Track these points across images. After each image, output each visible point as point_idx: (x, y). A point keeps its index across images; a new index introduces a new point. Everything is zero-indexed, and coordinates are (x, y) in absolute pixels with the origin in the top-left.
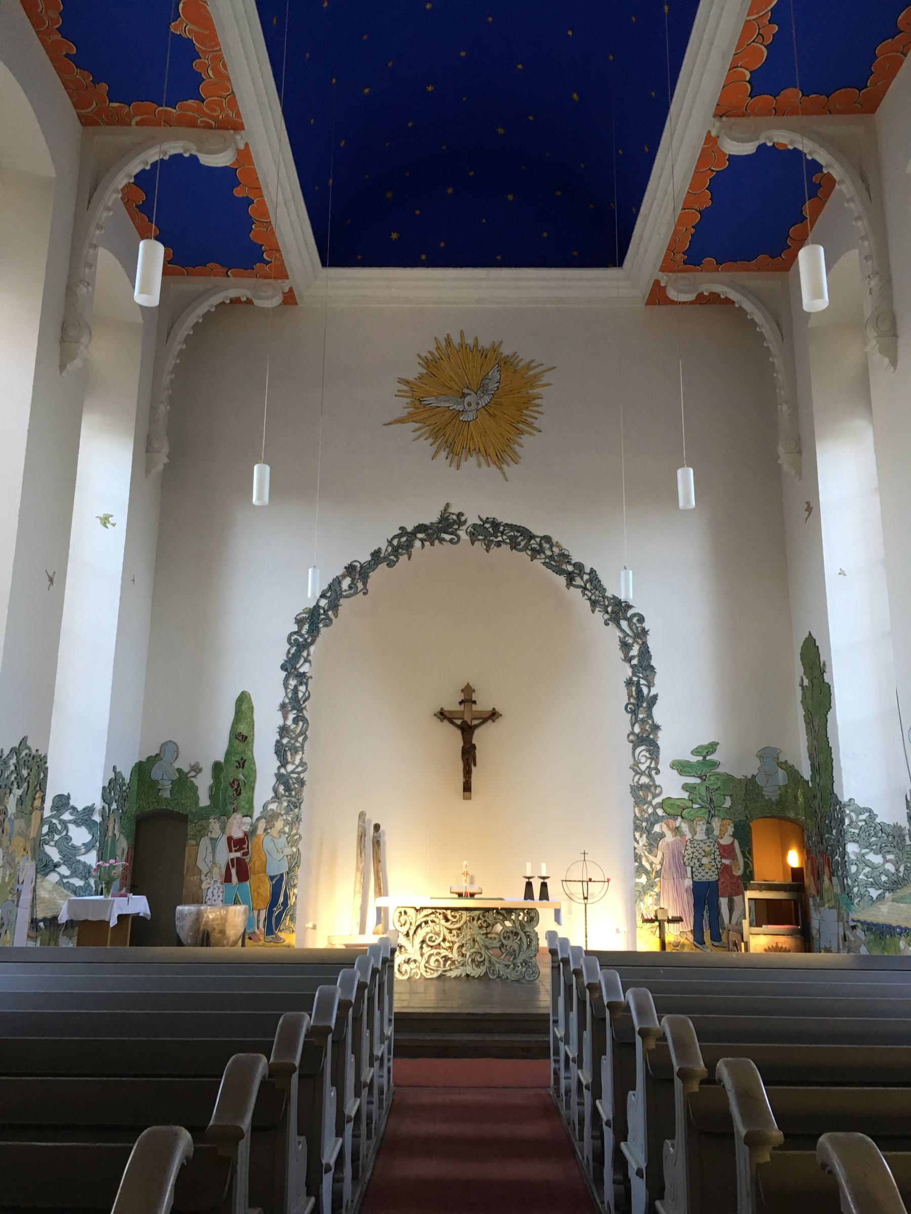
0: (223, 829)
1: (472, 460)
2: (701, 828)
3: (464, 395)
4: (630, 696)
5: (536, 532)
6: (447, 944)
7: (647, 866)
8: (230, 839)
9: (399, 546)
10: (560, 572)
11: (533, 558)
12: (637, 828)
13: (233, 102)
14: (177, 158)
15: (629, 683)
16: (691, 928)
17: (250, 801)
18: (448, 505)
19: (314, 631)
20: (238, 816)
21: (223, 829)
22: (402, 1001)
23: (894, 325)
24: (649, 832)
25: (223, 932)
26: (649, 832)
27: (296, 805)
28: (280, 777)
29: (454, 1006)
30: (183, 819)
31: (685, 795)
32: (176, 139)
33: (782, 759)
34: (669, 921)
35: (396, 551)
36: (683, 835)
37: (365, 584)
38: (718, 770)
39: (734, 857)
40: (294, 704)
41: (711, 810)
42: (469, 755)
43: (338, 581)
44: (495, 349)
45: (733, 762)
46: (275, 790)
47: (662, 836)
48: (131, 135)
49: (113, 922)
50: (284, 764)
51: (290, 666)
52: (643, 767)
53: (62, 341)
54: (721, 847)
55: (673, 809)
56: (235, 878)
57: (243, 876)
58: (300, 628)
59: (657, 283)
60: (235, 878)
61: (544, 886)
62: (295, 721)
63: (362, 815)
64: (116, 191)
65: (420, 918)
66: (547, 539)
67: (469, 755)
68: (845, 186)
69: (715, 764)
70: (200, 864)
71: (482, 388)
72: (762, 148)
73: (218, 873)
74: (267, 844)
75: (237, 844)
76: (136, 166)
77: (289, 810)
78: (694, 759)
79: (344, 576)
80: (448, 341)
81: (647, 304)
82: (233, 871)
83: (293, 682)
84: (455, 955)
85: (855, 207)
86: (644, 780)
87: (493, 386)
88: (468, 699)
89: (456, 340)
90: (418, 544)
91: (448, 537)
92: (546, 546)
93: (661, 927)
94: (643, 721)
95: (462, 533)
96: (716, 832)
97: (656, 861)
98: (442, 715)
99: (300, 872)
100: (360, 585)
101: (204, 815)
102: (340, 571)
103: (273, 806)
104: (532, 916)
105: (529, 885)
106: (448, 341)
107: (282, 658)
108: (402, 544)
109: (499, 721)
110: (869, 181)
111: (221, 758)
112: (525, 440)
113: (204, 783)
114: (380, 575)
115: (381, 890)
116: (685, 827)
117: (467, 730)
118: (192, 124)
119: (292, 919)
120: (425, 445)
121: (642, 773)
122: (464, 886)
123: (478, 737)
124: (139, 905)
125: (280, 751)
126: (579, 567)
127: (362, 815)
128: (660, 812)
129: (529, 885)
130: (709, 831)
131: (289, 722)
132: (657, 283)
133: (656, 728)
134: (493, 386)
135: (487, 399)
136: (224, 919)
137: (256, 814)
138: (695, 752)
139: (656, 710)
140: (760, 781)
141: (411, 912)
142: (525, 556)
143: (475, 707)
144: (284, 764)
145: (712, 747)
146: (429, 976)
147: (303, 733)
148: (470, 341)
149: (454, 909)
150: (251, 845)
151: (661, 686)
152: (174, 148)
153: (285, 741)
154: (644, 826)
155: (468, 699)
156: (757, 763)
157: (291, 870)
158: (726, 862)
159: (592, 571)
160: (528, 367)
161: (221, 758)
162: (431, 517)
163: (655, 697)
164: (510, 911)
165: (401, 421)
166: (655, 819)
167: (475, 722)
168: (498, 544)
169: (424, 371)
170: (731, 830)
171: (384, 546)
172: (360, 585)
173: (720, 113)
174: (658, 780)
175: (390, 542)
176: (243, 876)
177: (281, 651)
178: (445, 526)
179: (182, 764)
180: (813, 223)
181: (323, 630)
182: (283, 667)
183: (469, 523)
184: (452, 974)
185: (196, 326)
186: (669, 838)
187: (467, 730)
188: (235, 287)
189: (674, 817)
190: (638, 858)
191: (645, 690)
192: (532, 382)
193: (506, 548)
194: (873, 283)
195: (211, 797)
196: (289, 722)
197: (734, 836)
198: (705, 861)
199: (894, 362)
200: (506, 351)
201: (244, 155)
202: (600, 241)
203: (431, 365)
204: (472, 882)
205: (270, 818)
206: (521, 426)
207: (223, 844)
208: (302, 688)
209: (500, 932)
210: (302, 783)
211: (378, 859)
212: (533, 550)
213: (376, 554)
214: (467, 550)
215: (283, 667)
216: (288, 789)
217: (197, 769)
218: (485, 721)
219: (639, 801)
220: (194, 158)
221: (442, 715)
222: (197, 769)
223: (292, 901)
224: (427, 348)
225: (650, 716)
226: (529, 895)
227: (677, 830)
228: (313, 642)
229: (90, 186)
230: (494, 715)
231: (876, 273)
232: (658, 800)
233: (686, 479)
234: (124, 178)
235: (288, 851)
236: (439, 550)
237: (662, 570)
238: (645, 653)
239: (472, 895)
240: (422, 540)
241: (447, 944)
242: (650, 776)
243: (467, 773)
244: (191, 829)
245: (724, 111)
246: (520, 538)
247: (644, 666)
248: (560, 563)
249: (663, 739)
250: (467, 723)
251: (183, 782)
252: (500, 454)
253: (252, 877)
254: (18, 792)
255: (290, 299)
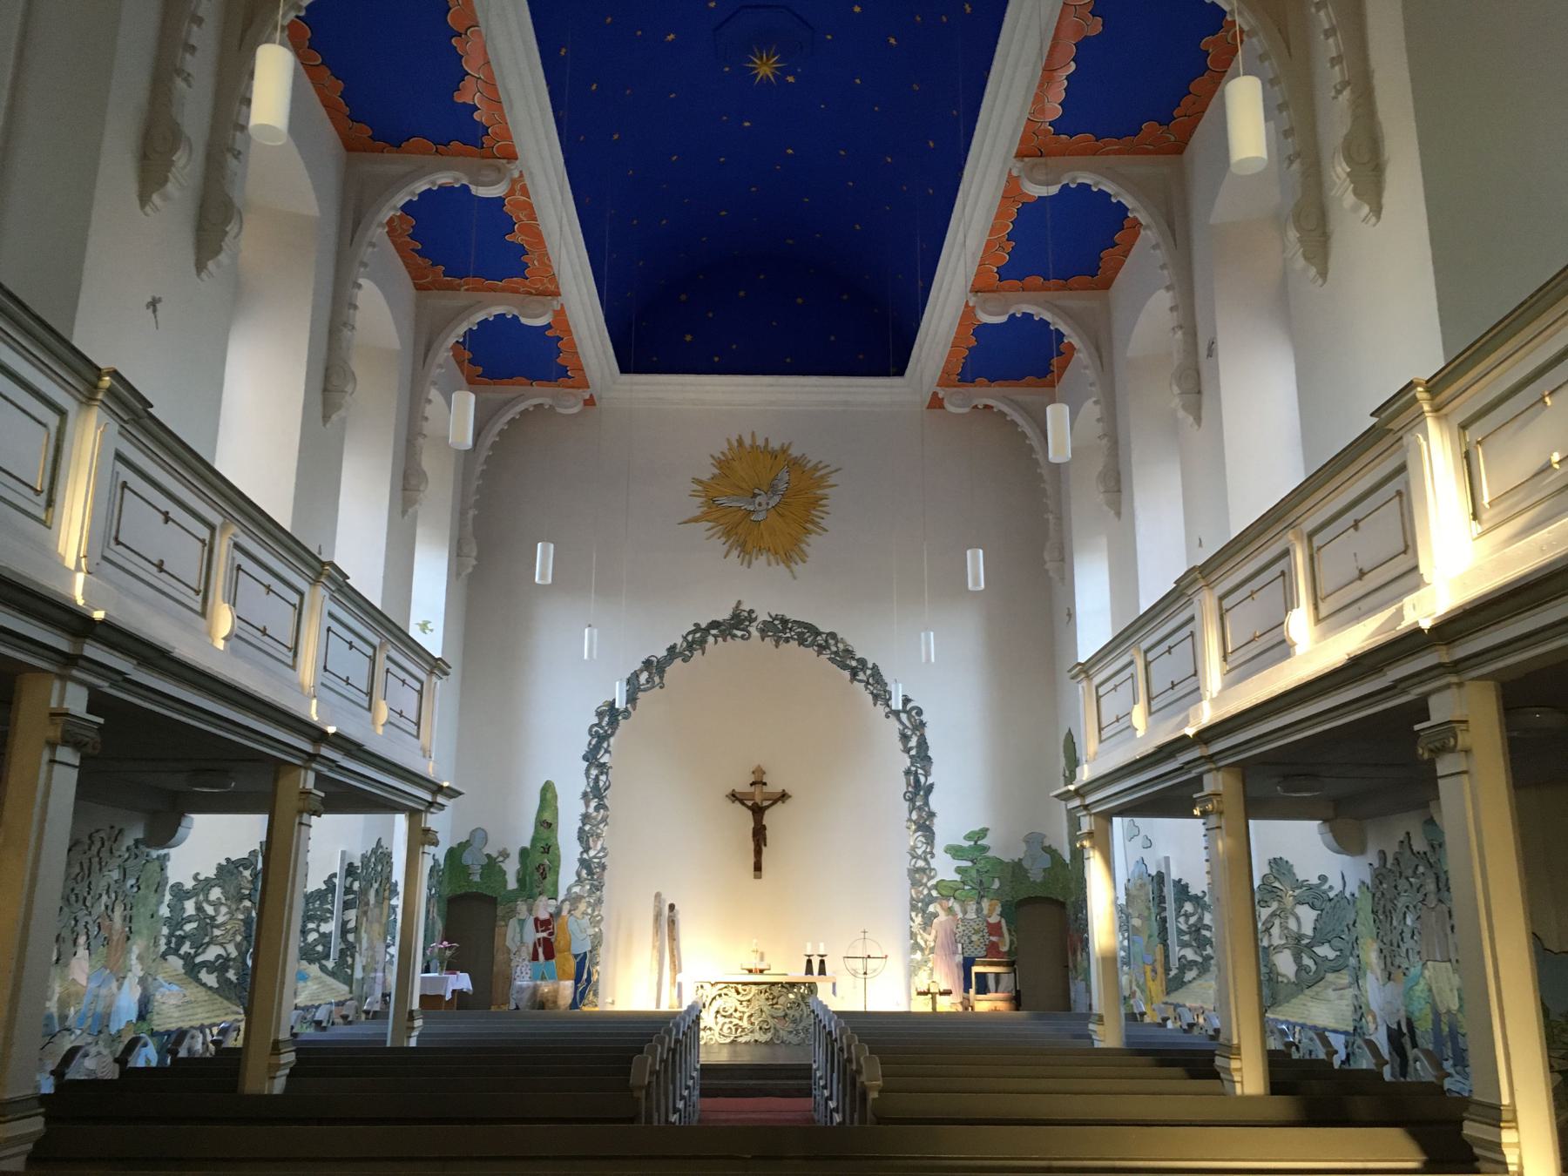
0: (530, 911)
1: (763, 558)
2: (972, 907)
3: (755, 496)
4: (908, 784)
5: (822, 629)
6: (737, 1015)
7: (922, 943)
8: (536, 920)
9: (694, 641)
10: (844, 667)
11: (819, 653)
12: (913, 908)
13: (553, 279)
14: (500, 317)
15: (908, 772)
16: (959, 1000)
17: (555, 884)
18: (739, 602)
19: (614, 723)
20: (543, 899)
21: (530, 911)
22: (705, 1058)
23: (1118, 481)
24: (924, 912)
25: (555, 1002)
26: (924, 912)
27: (597, 887)
28: (584, 863)
29: (745, 1058)
30: (492, 901)
31: (957, 877)
32: (448, 168)
33: (1047, 844)
34: (941, 994)
35: (690, 646)
36: (955, 915)
37: (661, 678)
38: (989, 854)
39: (1001, 935)
40: (596, 793)
41: (982, 891)
42: (759, 835)
43: (636, 675)
44: (784, 451)
45: (1002, 847)
46: (578, 874)
47: (936, 915)
48: (462, 298)
49: (448, 996)
50: (587, 850)
51: (591, 757)
52: (919, 852)
53: (325, 390)
54: (989, 925)
55: (947, 891)
56: (541, 956)
57: (550, 955)
58: (601, 720)
59: (935, 394)
60: (541, 956)
61: (822, 962)
62: (597, 809)
63: (658, 895)
64: (381, 225)
65: (714, 991)
66: (833, 635)
67: (759, 835)
68: (1082, 356)
69: (985, 849)
70: (509, 943)
71: (772, 489)
72: (1065, 187)
73: (526, 952)
74: (572, 925)
75: (542, 924)
76: (402, 199)
77: (591, 892)
78: (967, 844)
79: (641, 671)
80: (740, 442)
81: (929, 407)
82: (540, 950)
83: (594, 772)
84: (745, 1023)
85: (1090, 374)
86: (921, 863)
87: (782, 486)
88: (758, 783)
89: (748, 441)
90: (711, 639)
91: (739, 633)
92: (832, 642)
93: (934, 999)
94: (920, 808)
95: (753, 630)
96: (985, 912)
97: (931, 938)
98: (734, 797)
99: (601, 950)
100: (657, 679)
101: (513, 897)
102: (638, 666)
103: (576, 889)
104: (812, 988)
105: (809, 962)
106: (740, 442)
107: (584, 749)
108: (697, 640)
109: (788, 801)
110: (1102, 349)
111: (527, 844)
112: (813, 539)
113: (511, 868)
114: (676, 668)
115: (676, 967)
116: (957, 907)
117: (758, 811)
118: (515, 291)
119: (596, 994)
120: (719, 545)
121: (918, 857)
122: (754, 963)
123: (768, 819)
124: (463, 981)
125: (583, 837)
126: (862, 662)
127: (658, 895)
128: (934, 893)
129: (809, 962)
130: (979, 911)
131: (591, 810)
132: (935, 394)
133: (932, 815)
134: (782, 486)
135: (777, 499)
136: (556, 992)
137: (561, 897)
138: (968, 837)
139: (932, 798)
140: (1026, 865)
141: (707, 986)
142: (812, 652)
143: (766, 789)
144: (587, 850)
145: (983, 833)
146: (722, 1040)
147: (604, 820)
148: (760, 442)
149: (745, 984)
150: (556, 924)
151: (938, 775)
152: (444, 179)
153: (587, 828)
154: (919, 906)
155: (758, 783)
156: (1024, 847)
157: (594, 949)
158: (994, 939)
159: (875, 667)
160: (816, 468)
161: (527, 844)
162: (724, 615)
163: (932, 786)
164: (793, 985)
165: (696, 520)
166: (932, 900)
167: (766, 803)
168: (787, 640)
169: (717, 471)
170: (998, 909)
171: (679, 641)
172: (657, 679)
173: (975, 290)
174: (934, 863)
175: (685, 638)
176: (550, 955)
177: (583, 742)
178: (738, 622)
179: (491, 849)
180: (1060, 377)
181: (622, 722)
182: (585, 758)
183: (760, 619)
184: (742, 1040)
185: (501, 433)
186: (943, 917)
187: (758, 811)
188: (537, 395)
189: (947, 898)
190: (913, 935)
191: (922, 779)
192: (820, 482)
193: (794, 644)
194: (1105, 441)
195: (519, 881)
196: (591, 810)
197: (1001, 915)
198: (974, 938)
199: (1377, 210)
200: (795, 452)
201: (560, 314)
202: (886, 353)
203: (724, 464)
204: (762, 959)
205: (575, 900)
206: (809, 526)
207: (530, 925)
208: (603, 778)
209: (791, 1001)
210: (603, 867)
211: (673, 938)
212: (819, 646)
213: (672, 649)
214: (756, 645)
215: (585, 758)
216: (590, 873)
217: (505, 854)
218: (775, 802)
219: (915, 883)
220: (465, 188)
221: (734, 797)
222: (505, 854)
223: (595, 977)
224: (720, 448)
225: (926, 803)
226: (809, 971)
227: (950, 910)
228: (612, 734)
229: (424, 349)
230: (784, 796)
231: (1181, 327)
232: (933, 882)
233: (976, 563)
234: (391, 208)
235: (591, 931)
236: (733, 646)
237: (937, 665)
238: (923, 744)
239: (761, 971)
240: (715, 636)
241: (737, 1015)
242: (926, 860)
243: (758, 853)
244: (500, 911)
245: (1030, 150)
246: (807, 634)
247: (922, 756)
248: (846, 660)
249: (938, 825)
250: (758, 806)
251: (492, 867)
252: (789, 553)
253: (557, 955)
254: (376, 886)
255: (590, 402)
